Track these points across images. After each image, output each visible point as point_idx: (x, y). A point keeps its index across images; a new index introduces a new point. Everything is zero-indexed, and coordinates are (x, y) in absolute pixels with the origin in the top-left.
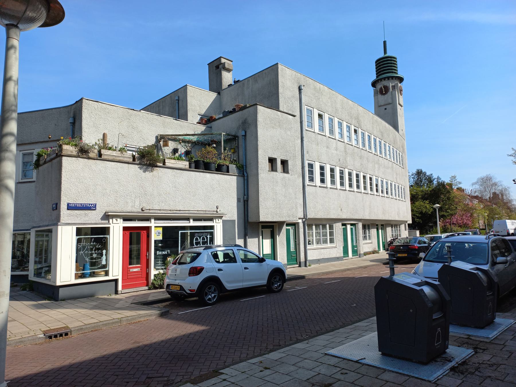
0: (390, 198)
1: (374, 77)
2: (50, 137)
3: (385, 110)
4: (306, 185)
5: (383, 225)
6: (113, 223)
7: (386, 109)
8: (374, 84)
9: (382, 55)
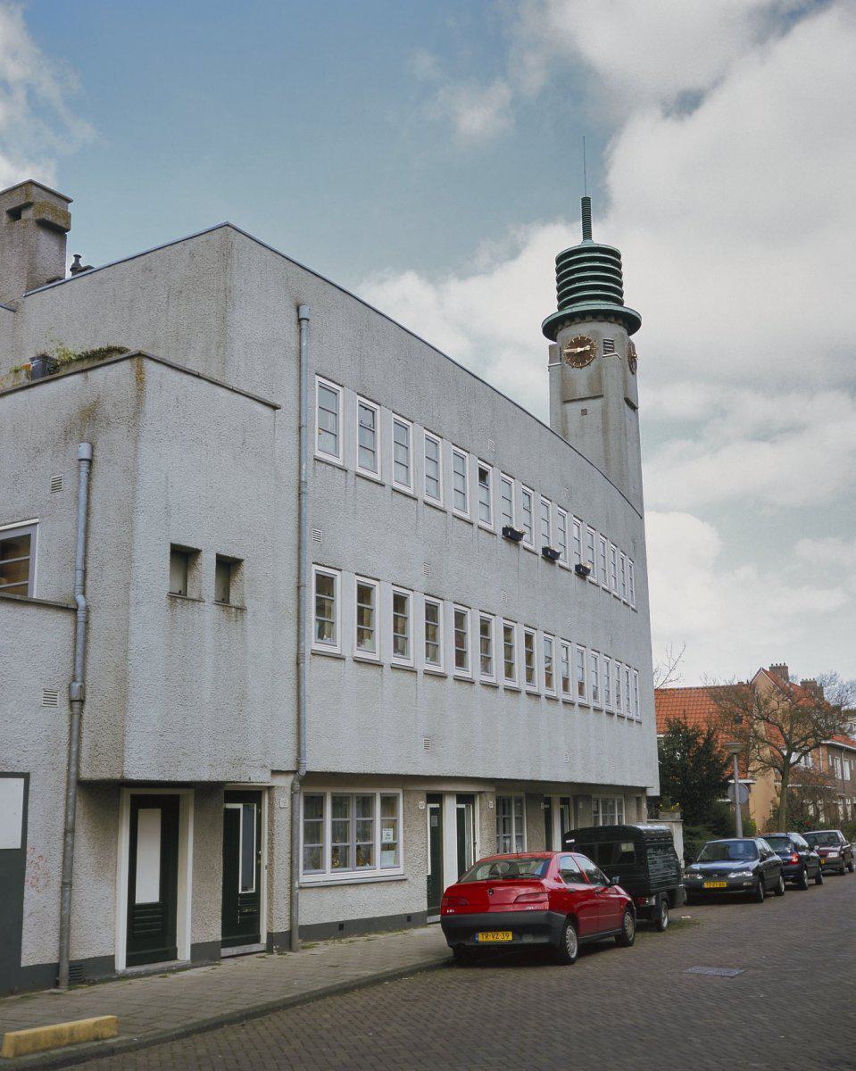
1: (550, 307)
3: (582, 415)
4: (308, 652)
5: (568, 799)
6: (22, 781)
7: (582, 410)
8: (551, 329)
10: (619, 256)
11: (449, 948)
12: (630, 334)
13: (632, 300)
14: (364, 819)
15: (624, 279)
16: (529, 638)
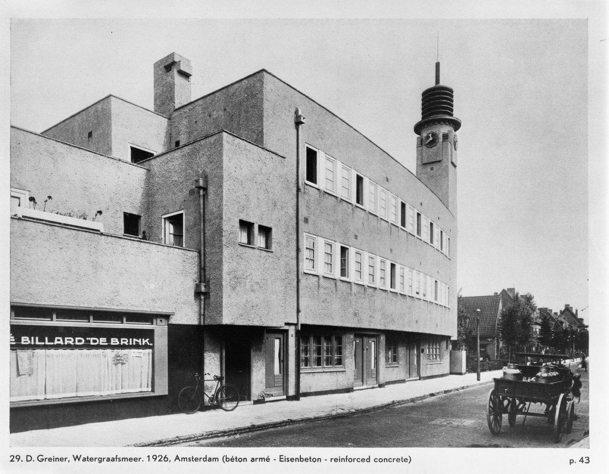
0: (422, 301)
1: (418, 118)
2: (479, 310)
8: (418, 129)
9: (432, 84)
10: (452, 92)
11: (488, 429)
12: (455, 130)
13: (457, 114)
14: (478, 338)
15: (454, 103)
16: (393, 266)
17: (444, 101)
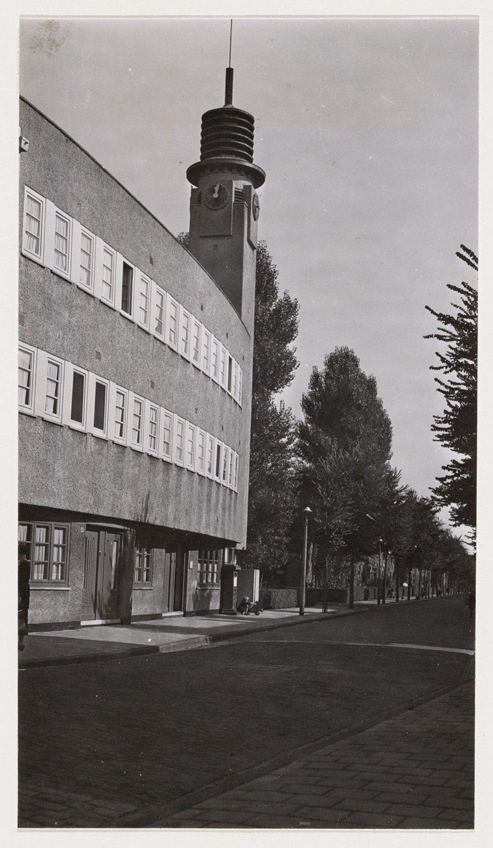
1: (196, 157)
8: (193, 174)
12: (256, 188)
13: (259, 160)
17: (240, 134)
